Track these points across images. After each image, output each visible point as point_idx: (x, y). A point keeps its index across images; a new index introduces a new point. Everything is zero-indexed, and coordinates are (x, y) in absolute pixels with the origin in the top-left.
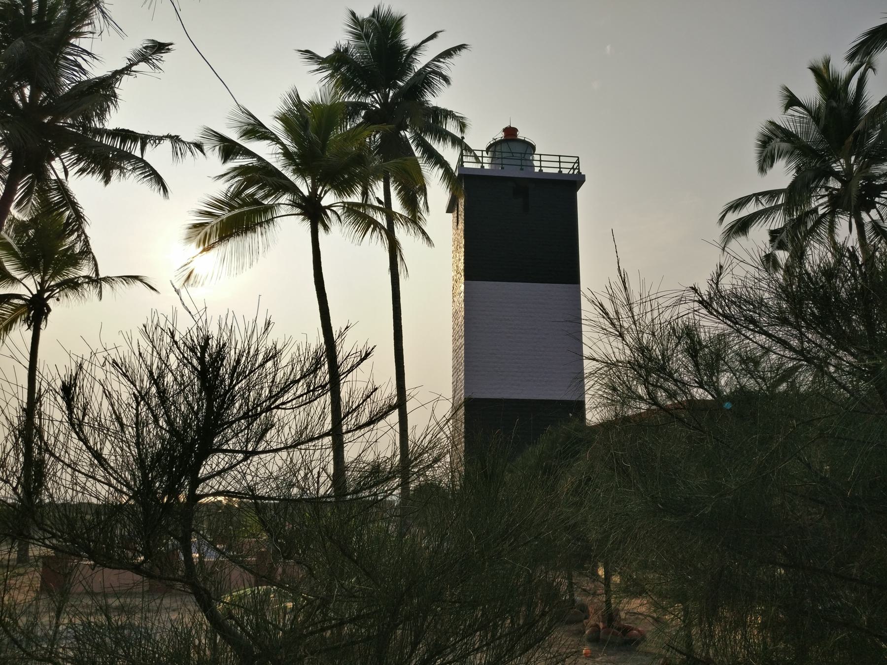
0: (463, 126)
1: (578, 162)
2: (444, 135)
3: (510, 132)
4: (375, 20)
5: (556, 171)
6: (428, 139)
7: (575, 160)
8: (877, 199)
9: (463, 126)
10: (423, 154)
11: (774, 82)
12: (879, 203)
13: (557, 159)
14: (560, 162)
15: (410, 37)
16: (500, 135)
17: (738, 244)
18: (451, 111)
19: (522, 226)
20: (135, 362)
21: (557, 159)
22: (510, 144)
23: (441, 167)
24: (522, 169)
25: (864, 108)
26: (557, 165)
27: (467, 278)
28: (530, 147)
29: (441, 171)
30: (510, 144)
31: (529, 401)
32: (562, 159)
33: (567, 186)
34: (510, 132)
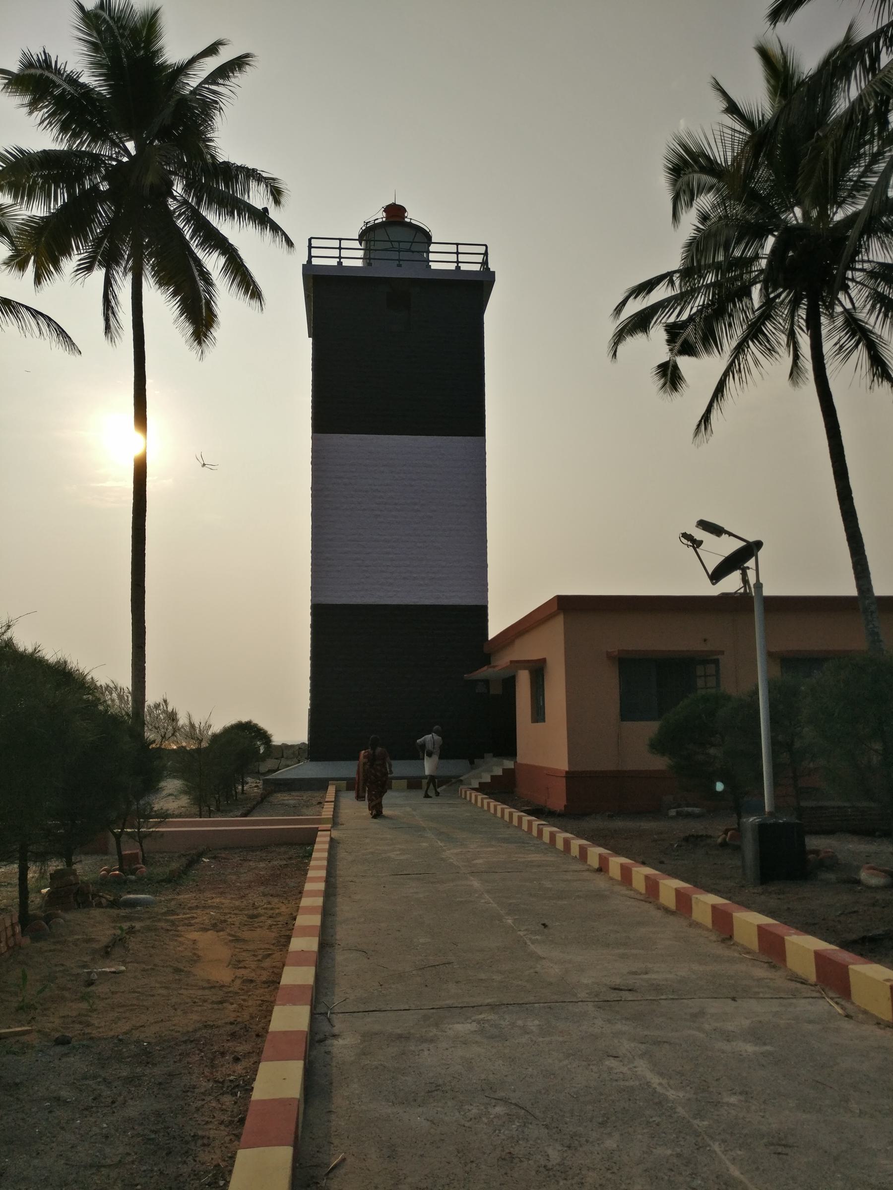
0: (276, 194)
1: (486, 254)
2: (236, 207)
3: (395, 212)
4: (105, 15)
5: (452, 267)
6: (212, 218)
7: (482, 250)
8: (849, 274)
9: (276, 194)
10: (15, 197)
11: (709, 93)
12: (853, 280)
13: (453, 248)
14: (457, 253)
15: (174, 49)
16: (381, 216)
17: (634, 343)
18: (254, 170)
19: (399, 352)
20: (197, 726)
21: (453, 248)
22: (394, 232)
23: (223, 253)
24: (399, 266)
25: (158, 59)
26: (453, 258)
27: (323, 422)
28: (424, 237)
29: (222, 260)
30: (394, 232)
31: (314, 527)
32: (462, 249)
33: (475, 288)
34: (395, 212)
